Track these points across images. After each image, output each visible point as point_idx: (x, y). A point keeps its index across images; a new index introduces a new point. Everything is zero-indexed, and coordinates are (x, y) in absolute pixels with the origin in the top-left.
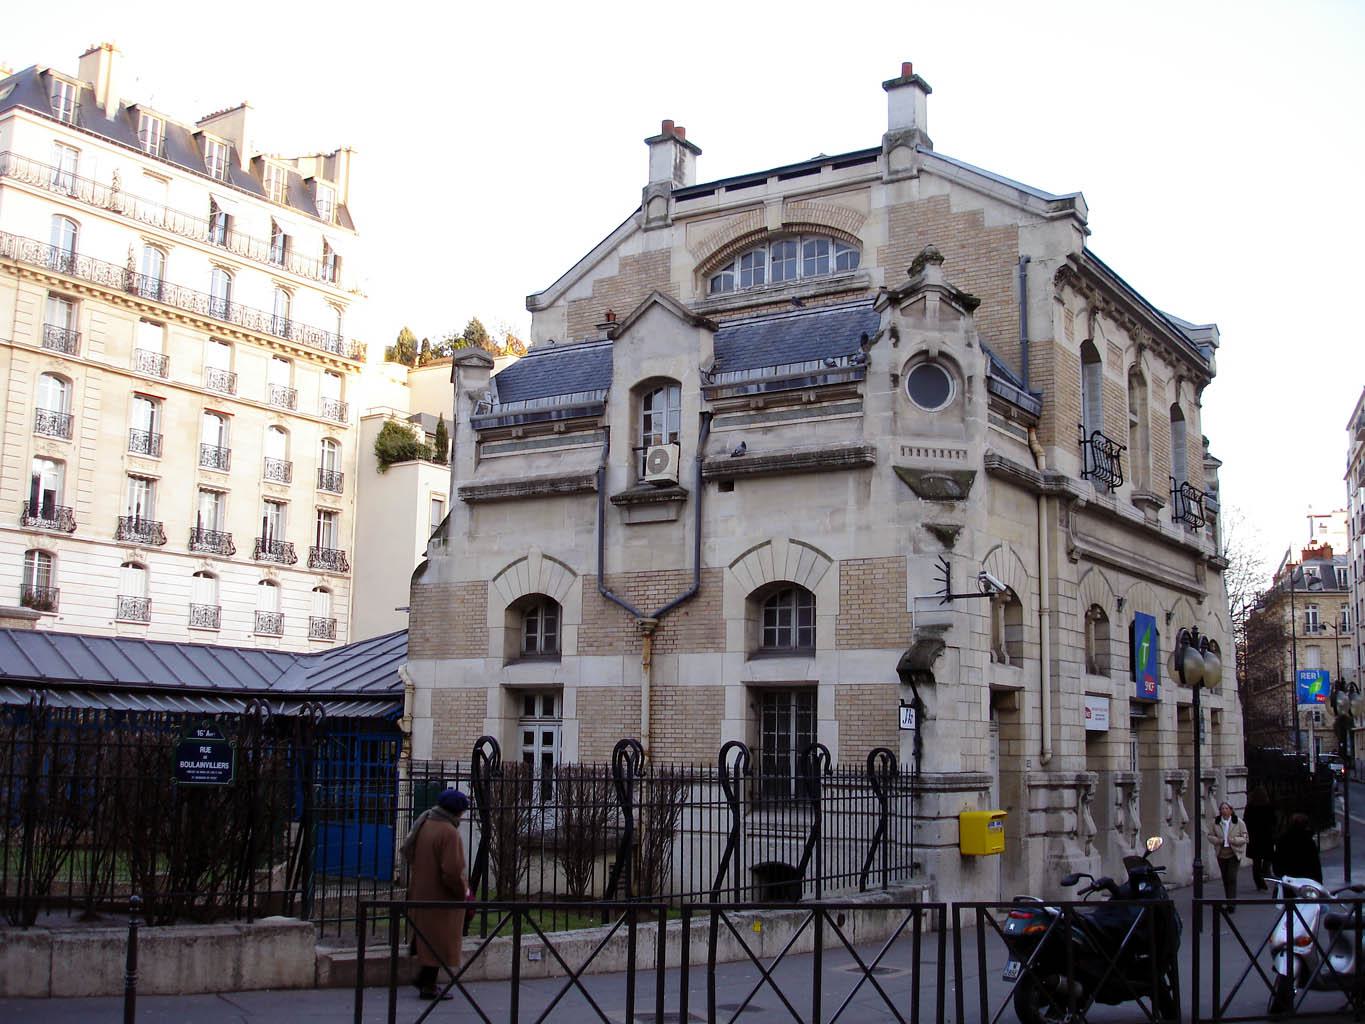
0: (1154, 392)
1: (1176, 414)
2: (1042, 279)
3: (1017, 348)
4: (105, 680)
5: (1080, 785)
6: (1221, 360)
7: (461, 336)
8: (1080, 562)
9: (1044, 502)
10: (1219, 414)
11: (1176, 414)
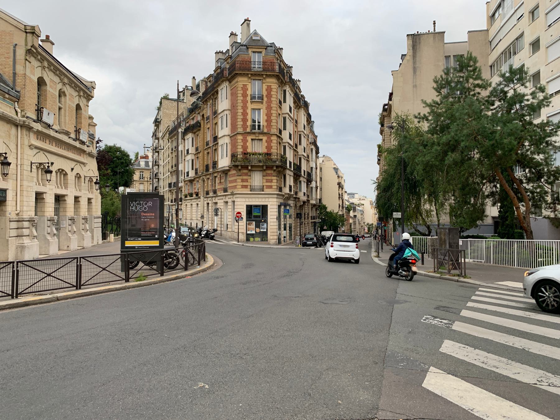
0: (69, 99)
1: (78, 107)
2: (21, 53)
3: (12, 75)
4: (120, 264)
5: (31, 221)
6: (96, 93)
7: (328, 210)
8: (34, 150)
9: (19, 128)
10: (93, 108)
11: (78, 107)
